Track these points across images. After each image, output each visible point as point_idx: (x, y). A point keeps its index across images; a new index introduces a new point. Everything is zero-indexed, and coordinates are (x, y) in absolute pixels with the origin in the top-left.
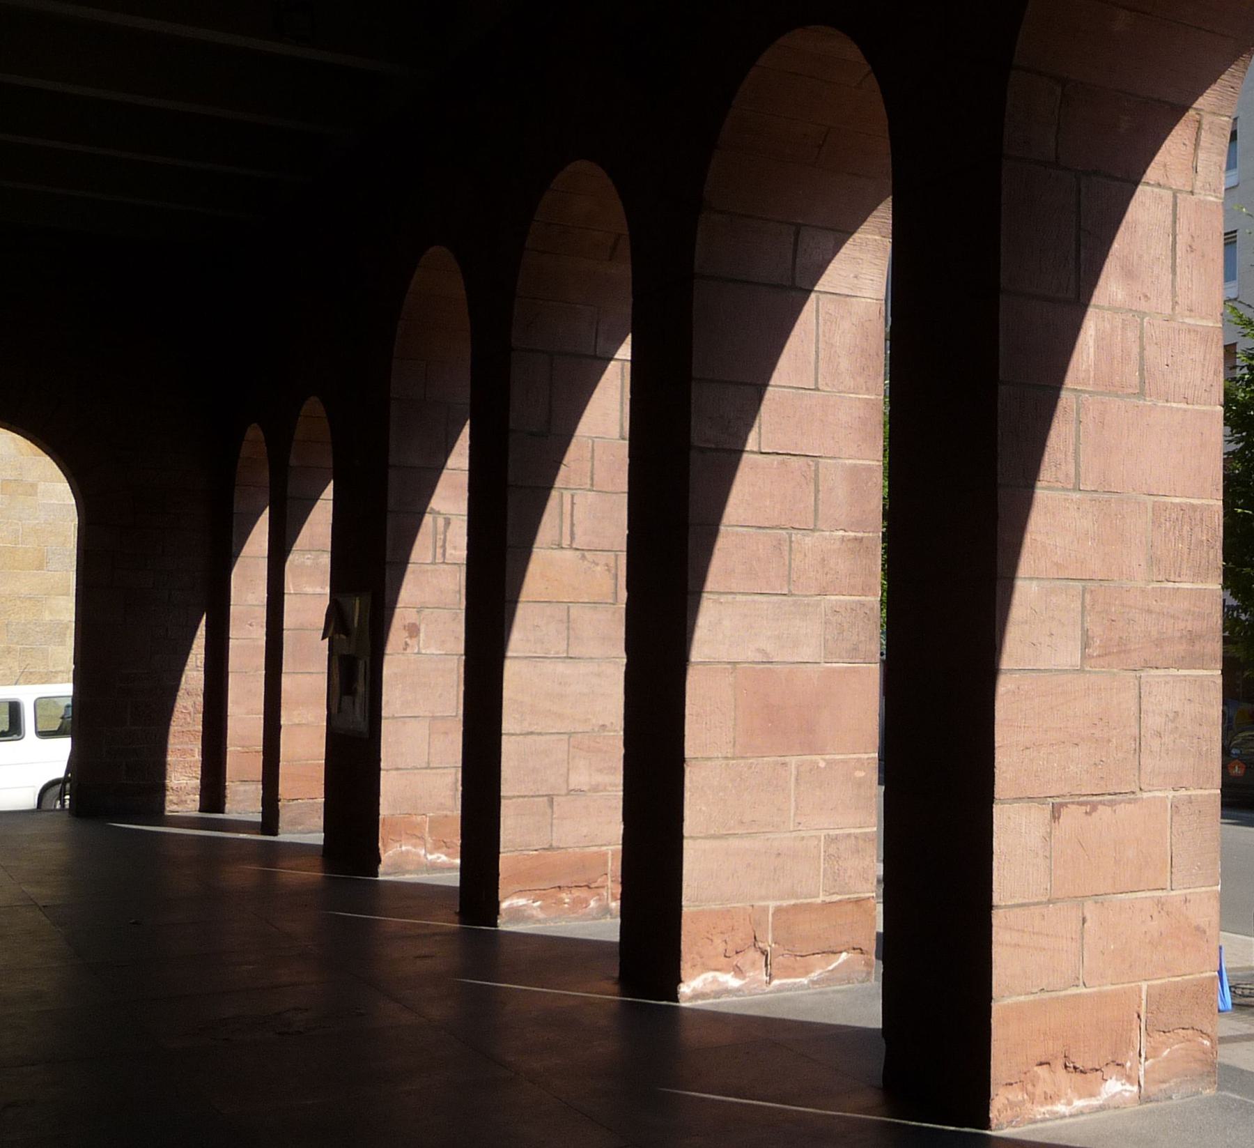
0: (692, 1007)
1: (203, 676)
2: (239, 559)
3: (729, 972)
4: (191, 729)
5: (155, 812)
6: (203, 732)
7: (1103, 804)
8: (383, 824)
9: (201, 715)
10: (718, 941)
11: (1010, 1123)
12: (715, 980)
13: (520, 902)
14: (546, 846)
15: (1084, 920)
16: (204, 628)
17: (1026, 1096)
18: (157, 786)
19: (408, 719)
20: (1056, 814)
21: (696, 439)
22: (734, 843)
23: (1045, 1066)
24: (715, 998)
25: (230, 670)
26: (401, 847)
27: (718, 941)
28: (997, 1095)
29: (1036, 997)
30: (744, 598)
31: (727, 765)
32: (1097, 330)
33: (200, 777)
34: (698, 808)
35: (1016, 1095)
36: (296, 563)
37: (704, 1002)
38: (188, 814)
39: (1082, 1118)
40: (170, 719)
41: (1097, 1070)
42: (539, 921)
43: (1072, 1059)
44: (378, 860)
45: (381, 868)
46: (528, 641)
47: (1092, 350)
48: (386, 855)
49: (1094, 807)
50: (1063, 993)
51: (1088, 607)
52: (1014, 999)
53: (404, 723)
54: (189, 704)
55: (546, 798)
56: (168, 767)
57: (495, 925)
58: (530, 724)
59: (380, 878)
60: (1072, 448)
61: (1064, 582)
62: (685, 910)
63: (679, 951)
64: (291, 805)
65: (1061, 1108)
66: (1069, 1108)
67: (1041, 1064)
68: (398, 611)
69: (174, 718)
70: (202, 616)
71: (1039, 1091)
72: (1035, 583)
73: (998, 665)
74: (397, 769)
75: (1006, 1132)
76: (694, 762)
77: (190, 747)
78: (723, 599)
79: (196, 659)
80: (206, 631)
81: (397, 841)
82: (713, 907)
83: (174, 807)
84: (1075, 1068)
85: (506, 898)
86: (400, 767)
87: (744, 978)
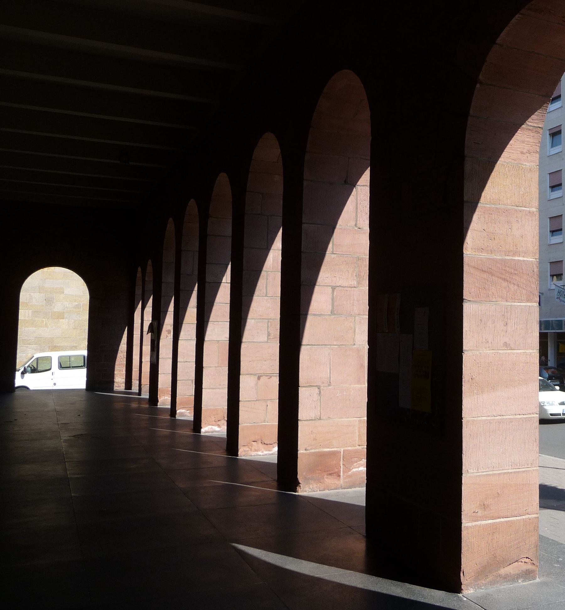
0: (209, 435)
1: (126, 346)
2: (137, 309)
3: (216, 426)
4: (122, 363)
5: (111, 389)
6: (126, 364)
7: (274, 376)
8: (160, 390)
9: (125, 359)
10: (213, 417)
11: (244, 456)
12: (212, 428)
13: (183, 411)
14: (191, 395)
15: (267, 406)
16: (127, 331)
17: (249, 449)
18: (112, 382)
19: (167, 359)
20: (259, 378)
21: (207, 280)
22: (218, 390)
23: (255, 442)
24: (212, 433)
25: (134, 344)
26: (165, 397)
27: (213, 417)
28: (240, 448)
29: (253, 424)
30: (221, 323)
31: (216, 369)
32: (273, 256)
33: (125, 378)
34: (207, 380)
35: (246, 449)
36: (148, 311)
37: (208, 434)
38: (120, 390)
39: (266, 456)
40: (116, 360)
41: (271, 444)
42: (188, 416)
43: (263, 441)
44: (158, 401)
45: (159, 404)
46: (186, 335)
47: (271, 261)
48: (160, 400)
49: (271, 377)
50: (261, 424)
51: (270, 326)
52: (246, 424)
53: (166, 360)
54: (122, 355)
55: (191, 381)
56: (115, 375)
57: (175, 417)
58: (186, 359)
59: (158, 407)
60: (265, 286)
61: (262, 320)
62: (203, 408)
63: (201, 420)
64: (145, 387)
65: (260, 453)
66: (263, 453)
67: (254, 441)
68: (164, 326)
69: (117, 360)
70: (126, 327)
71: (253, 448)
72: (253, 320)
73: (301, 343)
74: (164, 374)
75: (243, 458)
76: (206, 368)
77: (122, 369)
78: (215, 323)
79: (124, 341)
80: (127, 332)
81: (164, 396)
82: (211, 408)
83: (117, 388)
84: (264, 443)
85: (178, 409)
86: (165, 373)
87: (221, 428)
